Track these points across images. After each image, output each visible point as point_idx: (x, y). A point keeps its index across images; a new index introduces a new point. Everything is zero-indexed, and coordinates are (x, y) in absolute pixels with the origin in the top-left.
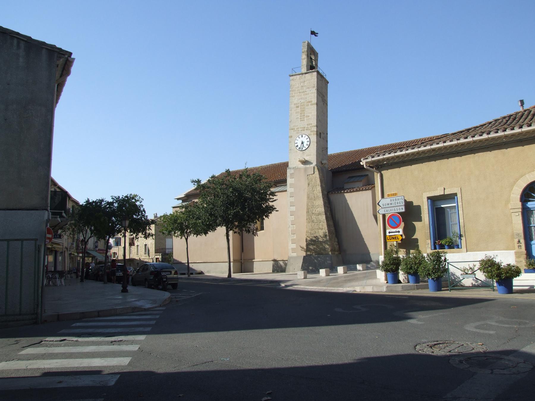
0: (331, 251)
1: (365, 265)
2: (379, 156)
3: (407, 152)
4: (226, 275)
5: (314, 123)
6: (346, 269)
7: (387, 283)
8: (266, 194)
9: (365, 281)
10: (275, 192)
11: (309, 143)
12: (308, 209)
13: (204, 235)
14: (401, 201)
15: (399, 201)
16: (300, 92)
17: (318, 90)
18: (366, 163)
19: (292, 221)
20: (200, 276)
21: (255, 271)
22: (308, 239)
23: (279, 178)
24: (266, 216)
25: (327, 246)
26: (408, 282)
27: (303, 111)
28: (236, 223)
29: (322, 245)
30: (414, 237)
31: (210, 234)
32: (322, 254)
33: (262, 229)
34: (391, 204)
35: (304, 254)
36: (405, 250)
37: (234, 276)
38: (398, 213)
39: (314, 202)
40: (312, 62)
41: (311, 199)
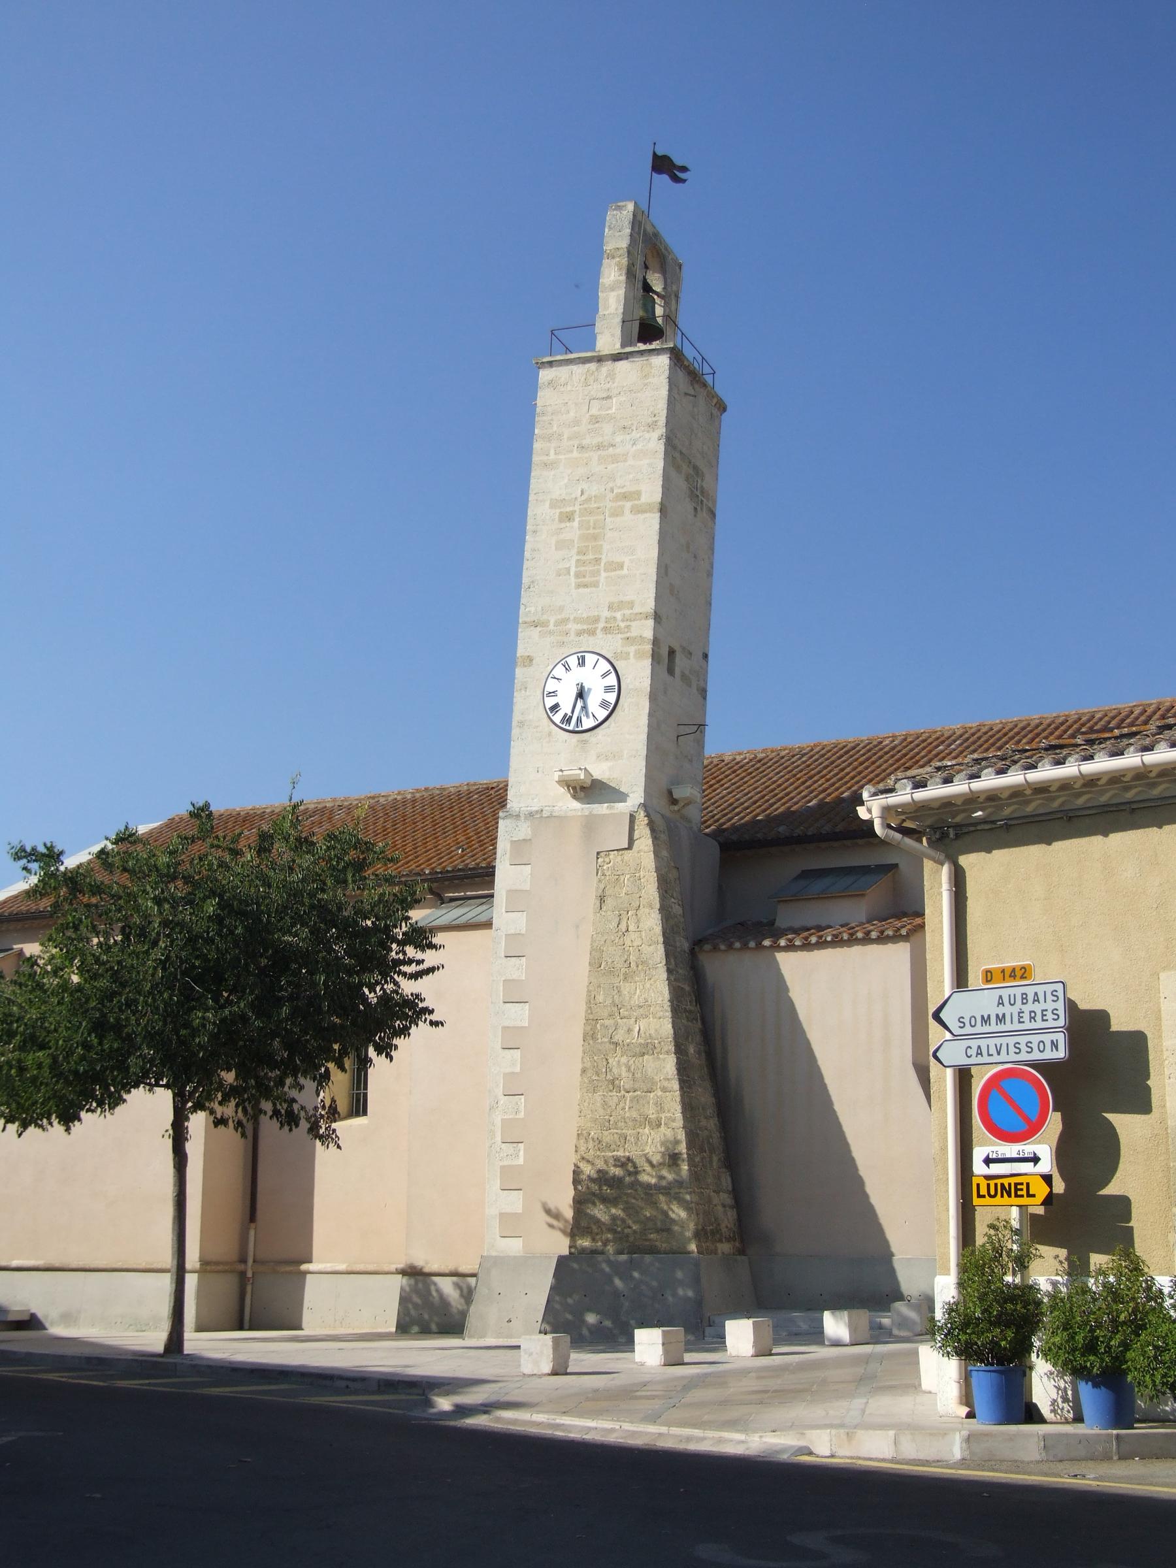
0: (699, 1235)
1: (863, 1316)
2: (948, 781)
3: (1089, 768)
4: (155, 1340)
5: (645, 597)
6: (768, 1332)
7: (971, 1415)
8: (384, 936)
9: (858, 1402)
10: (433, 930)
11: (611, 697)
12: (592, 1020)
13: (57, 1129)
14: (1050, 1006)
15: (1038, 1008)
16: (582, 447)
17: (670, 442)
18: (887, 810)
19: (510, 1077)
20: (19, 1342)
21: (312, 1323)
22: (587, 1170)
23: (459, 859)
24: (380, 1050)
25: (679, 1213)
26: (1078, 1419)
27: (595, 538)
28: (229, 1077)
29: (654, 1204)
30: (1111, 1189)
31: (90, 1121)
32: (653, 1250)
33: (359, 1107)
34: (1001, 1019)
35: (562, 1245)
36: (1063, 1253)
37: (201, 1344)
38: (1036, 1065)
39: (626, 988)
40: (649, 306)
41: (611, 972)
